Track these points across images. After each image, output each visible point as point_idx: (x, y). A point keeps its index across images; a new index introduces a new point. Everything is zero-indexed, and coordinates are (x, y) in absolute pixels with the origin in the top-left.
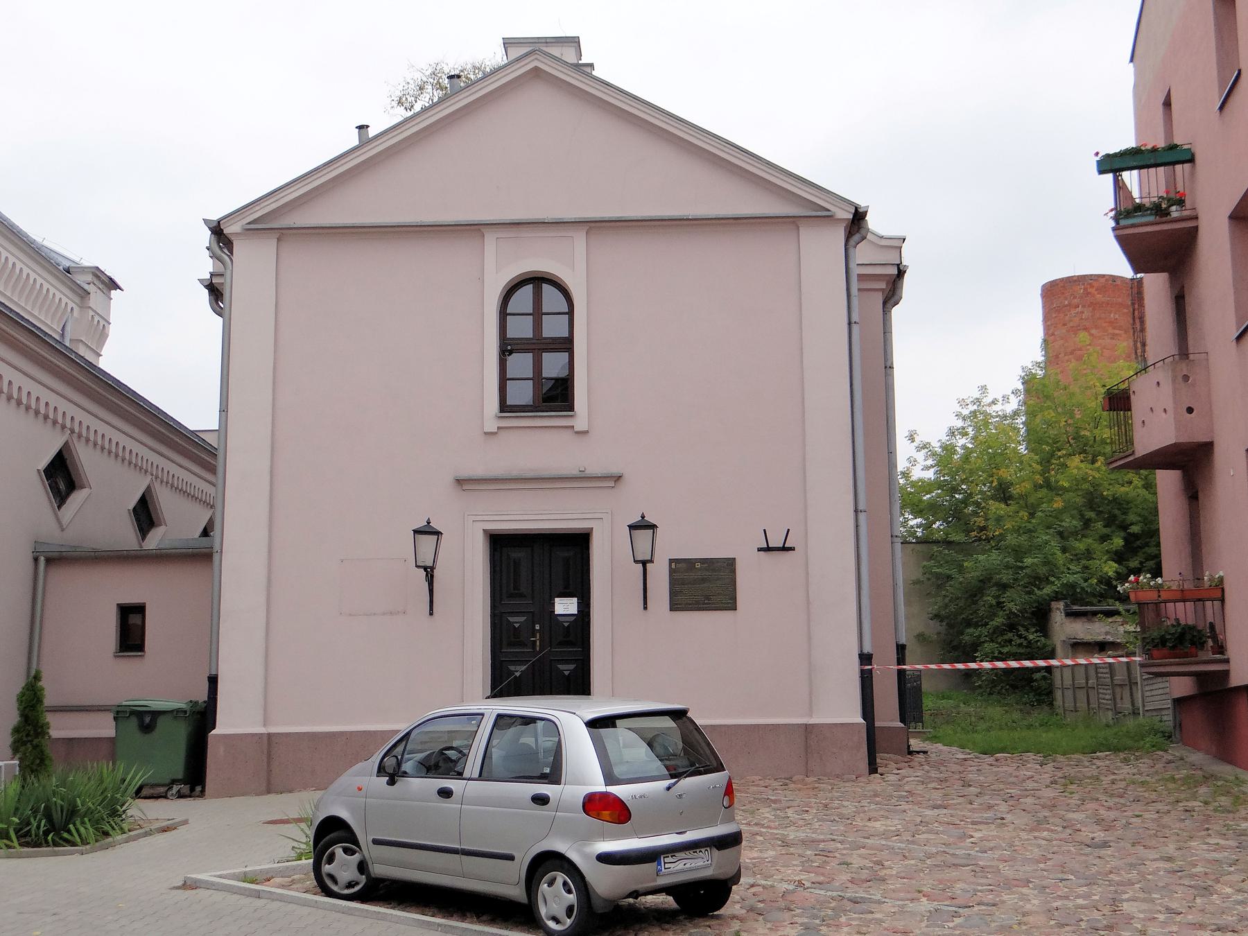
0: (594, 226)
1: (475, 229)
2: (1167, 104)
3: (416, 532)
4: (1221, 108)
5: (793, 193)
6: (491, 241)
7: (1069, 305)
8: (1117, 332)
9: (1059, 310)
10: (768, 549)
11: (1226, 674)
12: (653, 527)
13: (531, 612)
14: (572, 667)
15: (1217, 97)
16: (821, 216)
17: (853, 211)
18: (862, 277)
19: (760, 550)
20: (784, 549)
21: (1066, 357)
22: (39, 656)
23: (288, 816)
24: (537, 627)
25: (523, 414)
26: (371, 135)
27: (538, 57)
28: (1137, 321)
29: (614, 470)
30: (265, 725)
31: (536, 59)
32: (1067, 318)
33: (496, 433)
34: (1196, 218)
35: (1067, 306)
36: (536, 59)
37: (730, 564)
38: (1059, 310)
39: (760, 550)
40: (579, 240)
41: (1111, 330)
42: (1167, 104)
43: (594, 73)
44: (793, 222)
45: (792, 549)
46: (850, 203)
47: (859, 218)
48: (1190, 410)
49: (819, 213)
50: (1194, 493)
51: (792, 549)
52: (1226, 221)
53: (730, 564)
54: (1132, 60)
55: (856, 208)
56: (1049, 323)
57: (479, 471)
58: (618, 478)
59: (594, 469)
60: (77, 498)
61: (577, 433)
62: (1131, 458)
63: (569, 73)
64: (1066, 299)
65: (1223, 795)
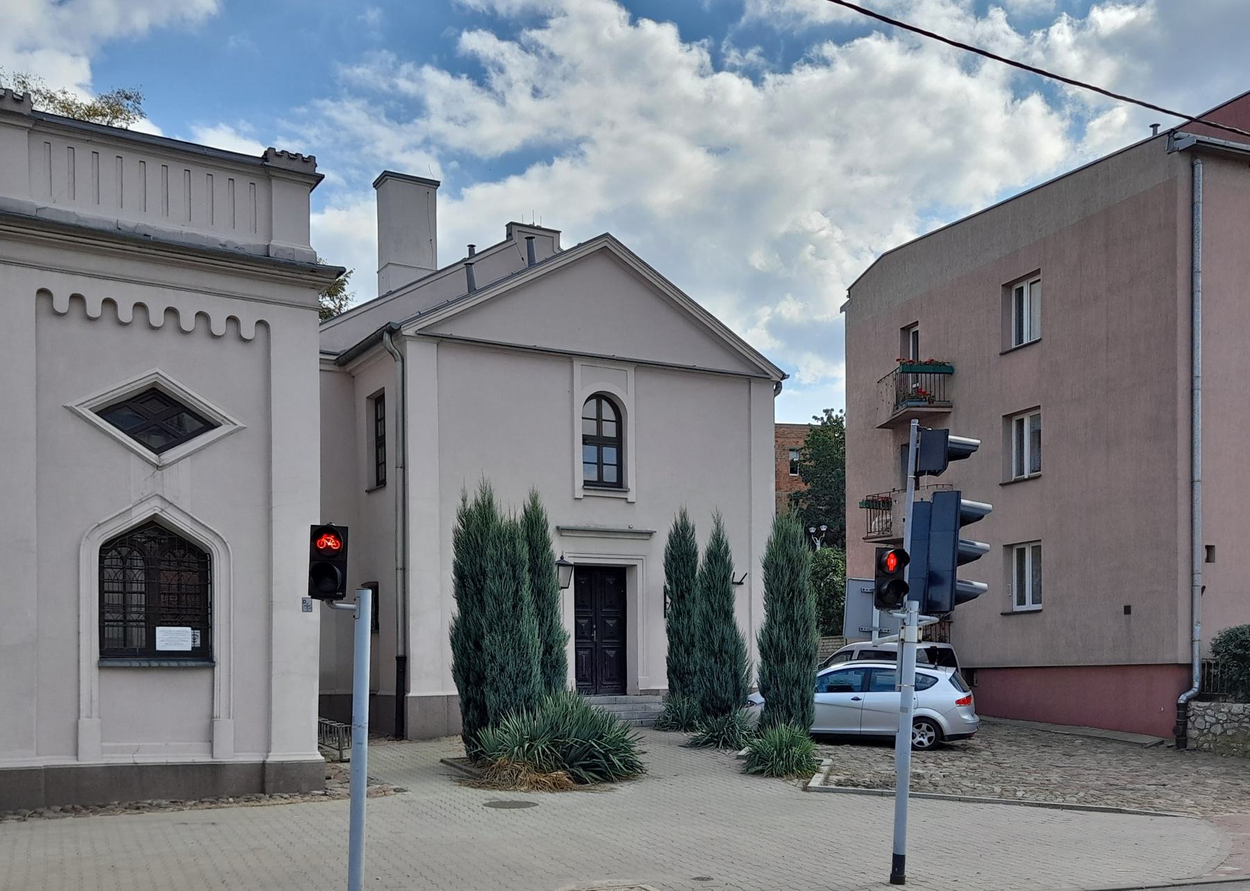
0: (639, 365)
1: (569, 356)
5: (631, 266)
13: (590, 617)
14: (614, 652)
18: (1021, 601)
23: (532, 809)
24: (594, 626)
26: (476, 252)
27: (607, 239)
29: (649, 529)
31: (606, 241)
33: (581, 499)
36: (606, 241)
40: (631, 372)
44: (749, 379)
49: (765, 376)
57: (572, 524)
58: (650, 534)
59: (637, 528)
61: (628, 502)
62: (890, 538)
63: (617, 247)
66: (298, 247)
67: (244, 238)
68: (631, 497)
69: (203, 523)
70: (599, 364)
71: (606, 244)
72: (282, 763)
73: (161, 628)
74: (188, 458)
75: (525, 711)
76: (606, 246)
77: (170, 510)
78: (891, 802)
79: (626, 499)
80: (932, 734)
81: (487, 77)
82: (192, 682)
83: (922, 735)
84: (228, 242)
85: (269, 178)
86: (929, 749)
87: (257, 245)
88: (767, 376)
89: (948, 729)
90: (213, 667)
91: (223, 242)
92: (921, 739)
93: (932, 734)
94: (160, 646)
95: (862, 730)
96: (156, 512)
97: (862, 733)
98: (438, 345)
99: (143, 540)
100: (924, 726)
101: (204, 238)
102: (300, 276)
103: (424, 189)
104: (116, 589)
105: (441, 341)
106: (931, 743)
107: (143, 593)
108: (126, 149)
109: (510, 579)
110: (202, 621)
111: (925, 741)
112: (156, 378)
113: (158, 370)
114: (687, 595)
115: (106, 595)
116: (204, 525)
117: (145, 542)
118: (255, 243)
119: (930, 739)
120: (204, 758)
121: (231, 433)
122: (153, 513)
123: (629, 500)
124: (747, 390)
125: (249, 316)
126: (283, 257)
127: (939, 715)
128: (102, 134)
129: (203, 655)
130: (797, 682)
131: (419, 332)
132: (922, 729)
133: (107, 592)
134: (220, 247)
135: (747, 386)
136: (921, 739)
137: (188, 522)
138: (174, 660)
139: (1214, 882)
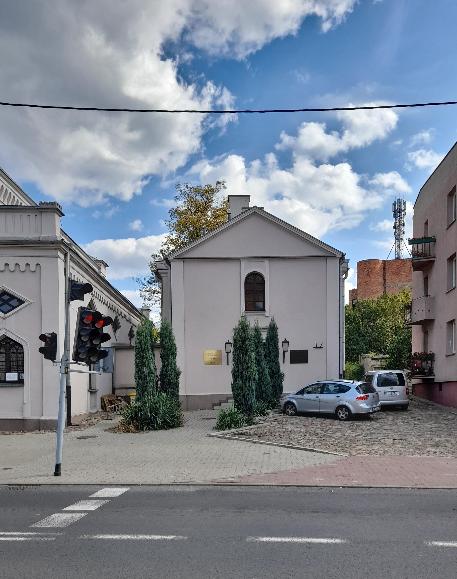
1: (238, 259)
2: (427, 223)
3: (226, 343)
4: (447, 229)
6: (242, 262)
7: (365, 268)
8: (378, 276)
9: (361, 270)
10: (316, 347)
11: (434, 379)
12: (288, 342)
15: (446, 225)
16: (334, 256)
17: (342, 255)
19: (314, 347)
20: (321, 347)
21: (363, 284)
22: (115, 374)
25: (255, 311)
28: (384, 273)
30: (185, 393)
32: (364, 272)
34: (435, 257)
35: (364, 269)
37: (306, 351)
38: (361, 270)
39: (314, 347)
40: (267, 262)
41: (376, 276)
42: (427, 223)
43: (264, 210)
44: (325, 258)
45: (323, 347)
46: (341, 252)
47: (343, 255)
48: (429, 311)
50: (426, 333)
51: (323, 347)
52: (446, 260)
53: (306, 351)
54: (414, 208)
55: (343, 254)
56: (359, 274)
60: (118, 331)
64: (364, 266)
65: (256, 386)
66: (50, 235)
67: (31, 235)
68: (267, 314)
69: (19, 336)
70: (252, 260)
71: (255, 211)
72: (46, 420)
73: (7, 373)
74: (14, 314)
75: (138, 401)
76: (255, 212)
77: (8, 333)
78: (55, 435)
79: (265, 315)
80: (347, 413)
81: (192, 154)
82: (15, 392)
83: (343, 413)
84: (27, 237)
85: (41, 212)
86: (346, 420)
87: (37, 237)
88: (335, 256)
89: (353, 411)
90: (24, 386)
91: (25, 238)
92: (343, 415)
93: (347, 413)
94: (7, 379)
95: (320, 411)
96: (4, 334)
97: (320, 412)
98: (183, 262)
99: (4, 343)
100: (344, 409)
101: (18, 237)
102: (48, 246)
103: (243, 199)
104: (15, 360)
105: (270, 259)
106: (341, 418)
107: (11, 361)
108: (7, 212)
109: (140, 351)
110: (20, 369)
111: (344, 416)
112: (3, 288)
113: (3, 285)
114: (272, 354)
115: (11, 362)
116: (19, 337)
117: (5, 344)
118: (37, 236)
119: (346, 415)
120: (20, 417)
121: (29, 304)
122: (2, 334)
123: (266, 315)
124: (326, 263)
125: (33, 262)
126: (45, 240)
127: (349, 404)
128: (6, 208)
129: (20, 382)
130: (242, 390)
131: (176, 258)
132: (343, 411)
133: (11, 361)
134: (24, 240)
135: (326, 261)
136: (343, 415)
137: (15, 337)
138: (10, 384)
139: (348, 487)
